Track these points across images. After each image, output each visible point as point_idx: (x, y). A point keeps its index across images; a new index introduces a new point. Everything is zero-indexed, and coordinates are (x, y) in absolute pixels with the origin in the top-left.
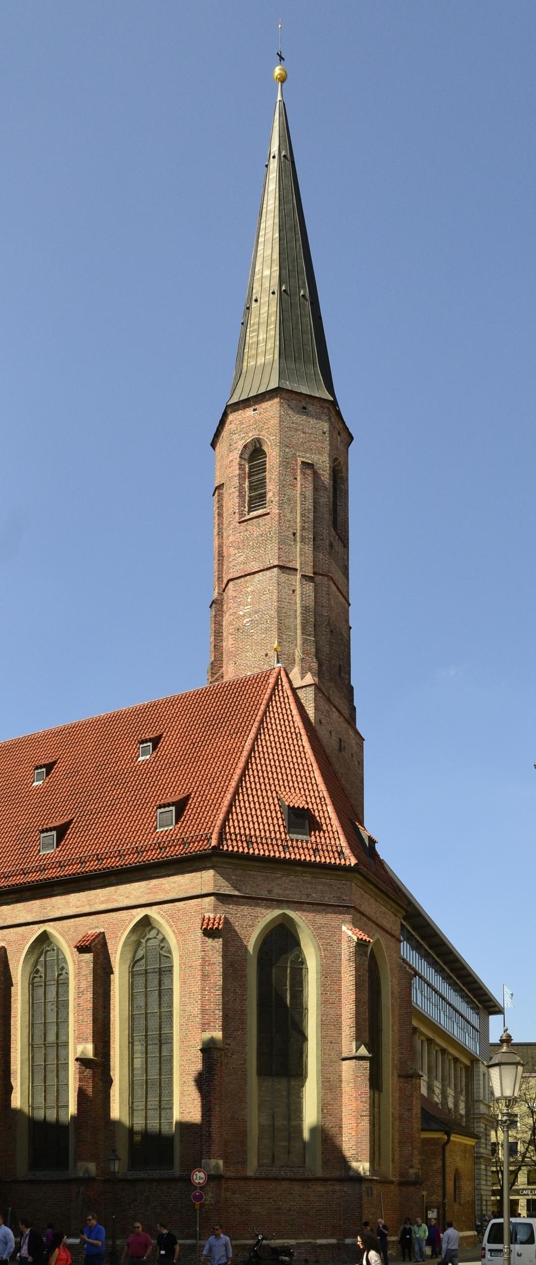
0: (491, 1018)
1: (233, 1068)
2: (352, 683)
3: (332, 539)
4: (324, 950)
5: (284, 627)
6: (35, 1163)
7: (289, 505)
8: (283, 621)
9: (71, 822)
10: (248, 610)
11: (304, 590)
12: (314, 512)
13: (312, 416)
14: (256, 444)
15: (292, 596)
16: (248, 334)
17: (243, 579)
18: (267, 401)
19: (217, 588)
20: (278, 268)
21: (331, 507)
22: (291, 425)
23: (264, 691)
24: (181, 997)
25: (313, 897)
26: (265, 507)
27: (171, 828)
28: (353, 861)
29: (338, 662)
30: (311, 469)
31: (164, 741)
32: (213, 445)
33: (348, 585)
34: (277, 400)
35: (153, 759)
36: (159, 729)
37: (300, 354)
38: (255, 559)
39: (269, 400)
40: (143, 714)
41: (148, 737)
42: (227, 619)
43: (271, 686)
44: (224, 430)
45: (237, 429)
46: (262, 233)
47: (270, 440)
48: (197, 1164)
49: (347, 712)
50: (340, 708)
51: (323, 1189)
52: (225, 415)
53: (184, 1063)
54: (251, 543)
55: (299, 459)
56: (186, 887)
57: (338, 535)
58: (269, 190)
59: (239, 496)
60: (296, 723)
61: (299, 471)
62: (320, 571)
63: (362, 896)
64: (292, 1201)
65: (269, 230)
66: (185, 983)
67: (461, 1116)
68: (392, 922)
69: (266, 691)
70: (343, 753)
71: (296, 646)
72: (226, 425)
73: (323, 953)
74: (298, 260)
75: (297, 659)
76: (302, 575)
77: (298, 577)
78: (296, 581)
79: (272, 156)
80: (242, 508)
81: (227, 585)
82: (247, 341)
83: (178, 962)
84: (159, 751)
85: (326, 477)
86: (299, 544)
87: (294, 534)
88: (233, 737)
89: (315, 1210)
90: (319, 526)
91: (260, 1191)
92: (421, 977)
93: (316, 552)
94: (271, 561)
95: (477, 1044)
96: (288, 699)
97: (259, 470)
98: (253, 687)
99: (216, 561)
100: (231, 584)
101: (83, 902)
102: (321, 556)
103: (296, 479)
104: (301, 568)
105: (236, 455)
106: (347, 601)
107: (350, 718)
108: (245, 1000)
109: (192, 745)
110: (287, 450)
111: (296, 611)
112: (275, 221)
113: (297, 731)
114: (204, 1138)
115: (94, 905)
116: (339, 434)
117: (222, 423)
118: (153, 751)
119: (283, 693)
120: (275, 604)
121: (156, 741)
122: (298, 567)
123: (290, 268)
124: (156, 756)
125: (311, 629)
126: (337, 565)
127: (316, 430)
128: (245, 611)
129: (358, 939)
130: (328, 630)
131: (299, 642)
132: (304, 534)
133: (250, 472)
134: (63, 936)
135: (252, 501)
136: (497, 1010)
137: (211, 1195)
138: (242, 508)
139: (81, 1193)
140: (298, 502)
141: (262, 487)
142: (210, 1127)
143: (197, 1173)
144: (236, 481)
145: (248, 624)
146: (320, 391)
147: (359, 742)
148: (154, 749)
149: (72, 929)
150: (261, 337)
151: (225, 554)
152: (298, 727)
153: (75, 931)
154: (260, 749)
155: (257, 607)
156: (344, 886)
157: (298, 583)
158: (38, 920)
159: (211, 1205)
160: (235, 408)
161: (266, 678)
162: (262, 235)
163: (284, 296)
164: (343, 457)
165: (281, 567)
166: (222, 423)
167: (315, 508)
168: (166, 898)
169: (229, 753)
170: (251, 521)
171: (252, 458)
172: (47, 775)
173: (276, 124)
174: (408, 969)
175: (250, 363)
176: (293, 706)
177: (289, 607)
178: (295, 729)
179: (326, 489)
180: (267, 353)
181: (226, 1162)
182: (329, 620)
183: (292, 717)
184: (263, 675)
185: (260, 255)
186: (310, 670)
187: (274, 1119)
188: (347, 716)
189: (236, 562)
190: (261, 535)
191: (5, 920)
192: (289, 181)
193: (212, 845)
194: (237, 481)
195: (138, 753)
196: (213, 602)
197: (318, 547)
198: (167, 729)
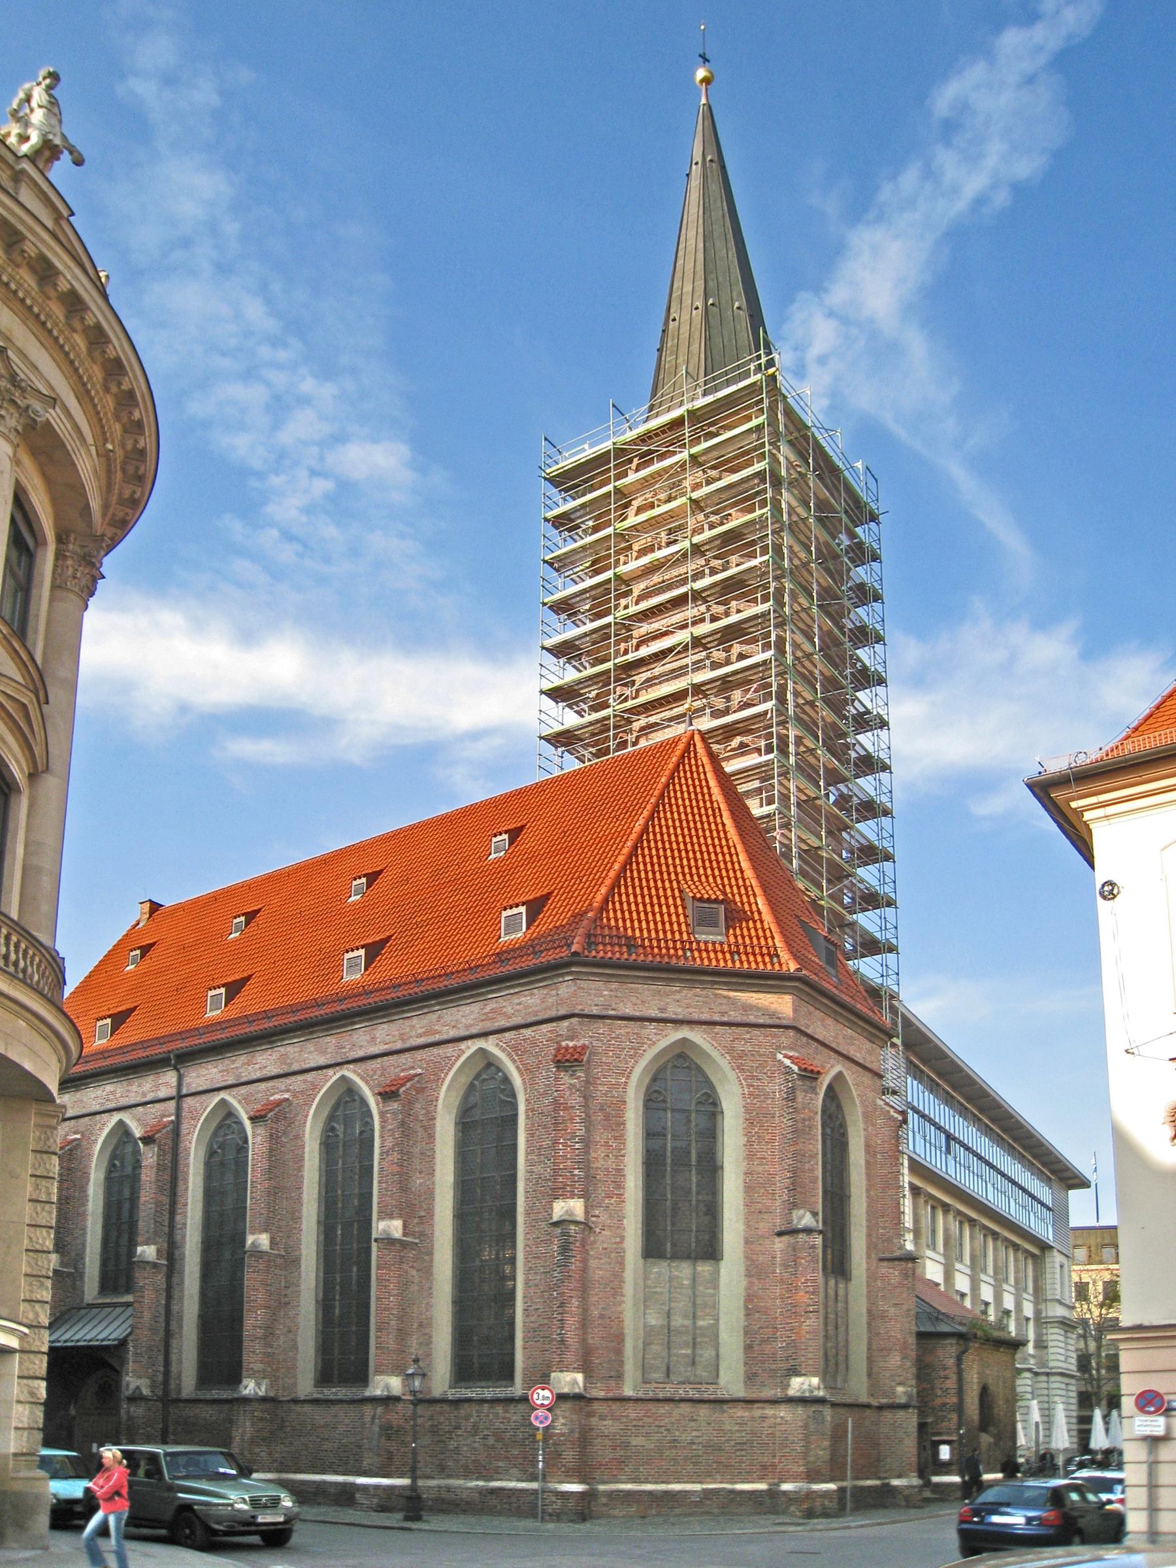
0: (1072, 1193)
4: (749, 1086)
6: (325, 1377)
24: (527, 1154)
25: (730, 1016)
28: (793, 967)
48: (544, 1380)
51: (746, 1414)
53: (529, 1243)
56: (536, 1009)
63: (810, 1013)
66: (532, 1135)
73: (746, 1090)
101: (394, 1036)
108: (623, 1156)
113: (715, 805)
115: (408, 1039)
119: (696, 760)
129: (800, 1069)
134: (367, 1082)
136: (1079, 1182)
137: (563, 1421)
142: (562, 1328)
143: (539, 1391)
149: (379, 1073)
152: (770, 929)
159: (563, 1435)
168: (508, 1025)
187: (669, 1317)
191: (290, 1065)
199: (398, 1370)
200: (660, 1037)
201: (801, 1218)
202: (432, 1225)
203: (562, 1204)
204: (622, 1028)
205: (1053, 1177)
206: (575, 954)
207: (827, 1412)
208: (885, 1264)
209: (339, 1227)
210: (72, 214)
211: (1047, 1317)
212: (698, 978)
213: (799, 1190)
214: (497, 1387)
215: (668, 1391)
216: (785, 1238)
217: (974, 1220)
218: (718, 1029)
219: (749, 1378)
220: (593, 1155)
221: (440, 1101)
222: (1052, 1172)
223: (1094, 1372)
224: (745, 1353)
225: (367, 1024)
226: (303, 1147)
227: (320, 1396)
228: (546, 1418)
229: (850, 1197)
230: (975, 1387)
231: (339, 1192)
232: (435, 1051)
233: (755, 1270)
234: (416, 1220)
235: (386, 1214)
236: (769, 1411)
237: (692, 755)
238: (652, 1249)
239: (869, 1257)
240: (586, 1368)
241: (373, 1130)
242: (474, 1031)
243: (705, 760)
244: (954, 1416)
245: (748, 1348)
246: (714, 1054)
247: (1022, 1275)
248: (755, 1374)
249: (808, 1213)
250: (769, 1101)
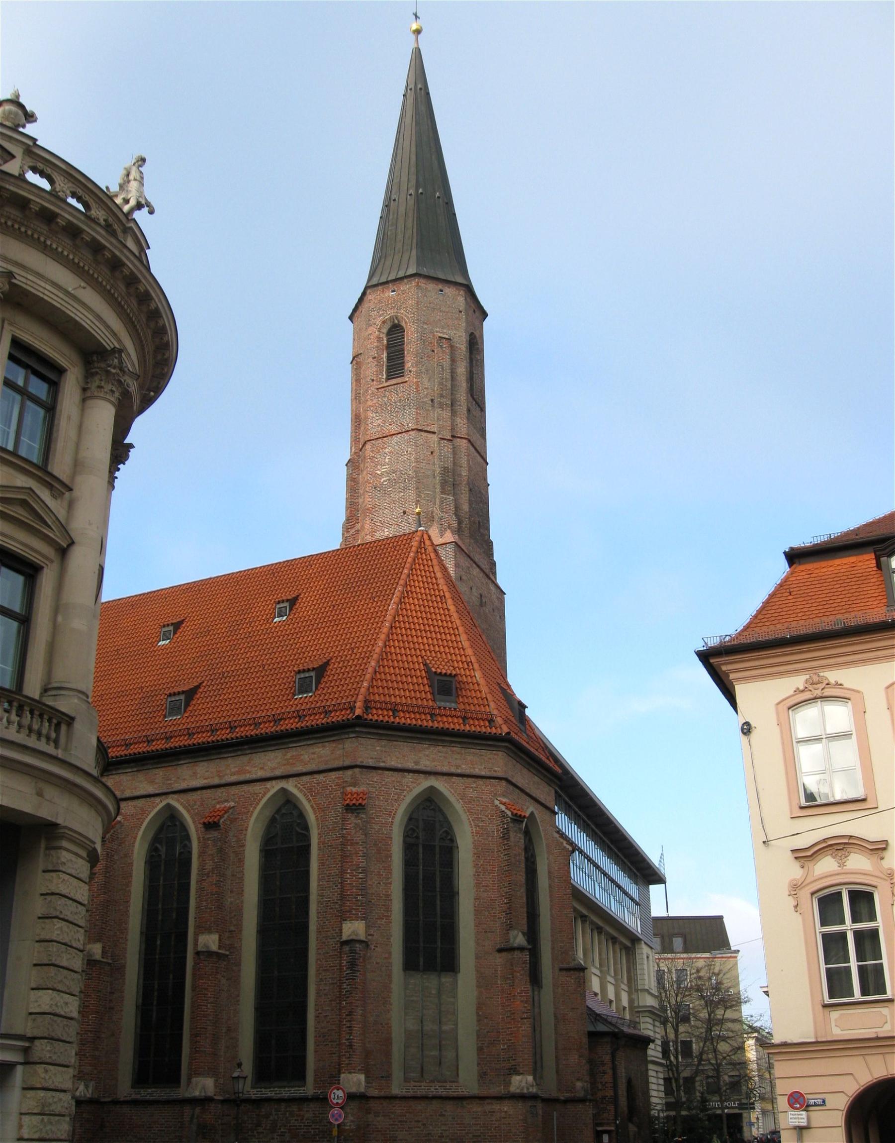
0: (652, 888)
1: (377, 963)
6: (141, 1078)
9: (198, 687)
24: (319, 880)
25: (462, 769)
26: (403, 376)
27: (310, 694)
33: (485, 446)
47: (408, 318)
50: (480, 564)
51: (479, 1109)
64: (445, 1125)
66: (323, 864)
67: (624, 1008)
68: (545, 793)
83: (317, 841)
89: (470, 1135)
91: (406, 1112)
92: (581, 852)
94: (410, 425)
95: (638, 920)
107: (489, 571)
108: (390, 884)
114: (344, 1047)
121: (293, 602)
129: (512, 813)
133: (388, 344)
134: (188, 811)
137: (352, 1118)
139: (195, 1116)
143: (335, 1091)
149: (198, 803)
153: (202, 804)
156: (496, 757)
158: (160, 791)
168: (304, 770)
171: (389, 333)
172: (175, 633)
174: (565, 845)
181: (369, 1077)
187: (422, 1022)
193: (356, 714)
199: (212, 1072)
200: (415, 785)
201: (515, 938)
202: (240, 939)
203: (349, 925)
204: (389, 777)
205: (638, 874)
206: (358, 717)
207: (540, 1105)
208: (564, 973)
209: (159, 937)
210: (149, 248)
211: (639, 1007)
212: (440, 738)
213: (514, 913)
214: (292, 1087)
215: (423, 1089)
216: (504, 954)
217: (586, 916)
218: (454, 779)
219: (481, 1077)
220: (370, 883)
221: (250, 829)
222: (638, 869)
223: (672, 1058)
224: (478, 1055)
225: (191, 761)
226: (131, 864)
227: (138, 1097)
228: (340, 1116)
229: (539, 916)
230: (624, 1081)
231: (160, 906)
232: (245, 787)
233: (483, 982)
234: (227, 934)
235: (202, 928)
236: (496, 1106)
238: (410, 965)
239: (553, 968)
240: (367, 1072)
241: (190, 853)
242: (278, 773)
244: (611, 1108)
245: (480, 1050)
246: (452, 799)
247: (604, 956)
248: (485, 1073)
249: (520, 933)
250: (490, 839)
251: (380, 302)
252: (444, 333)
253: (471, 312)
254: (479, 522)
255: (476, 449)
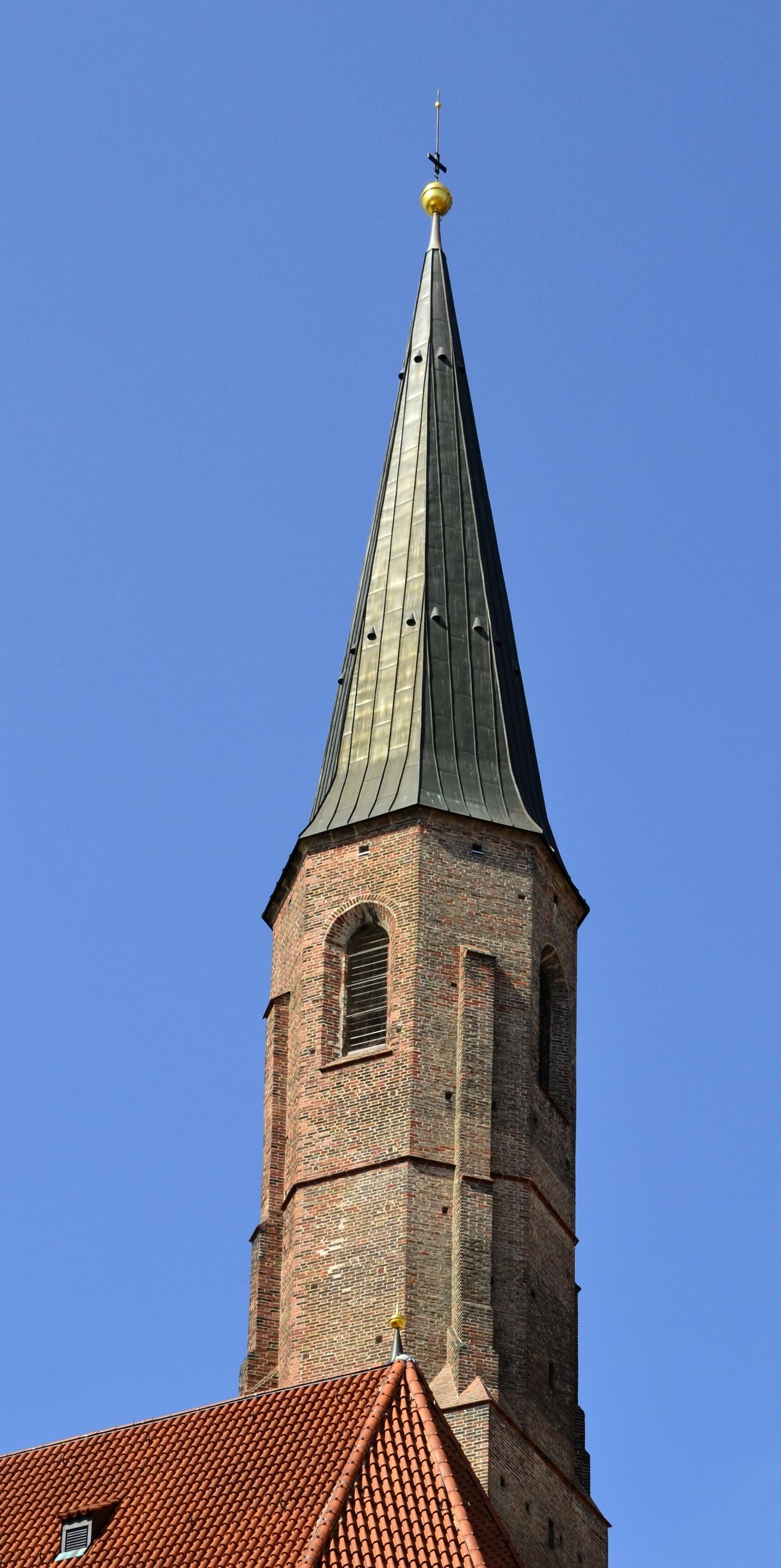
2: (581, 1403)
3: (536, 1107)
5: (422, 1284)
7: (438, 1037)
8: (419, 1270)
10: (339, 1247)
11: (469, 1207)
12: (496, 1052)
13: (494, 864)
14: (364, 917)
15: (441, 1221)
16: (352, 701)
17: (328, 1184)
18: (392, 831)
19: (267, 1202)
20: (423, 574)
21: (535, 1042)
22: (446, 879)
23: (366, 1410)
26: (383, 1042)
29: (547, 1358)
30: (488, 966)
31: (122, 1517)
32: (269, 917)
33: (572, 1201)
34: (413, 831)
35: (92, 1557)
36: (113, 1491)
37: (468, 741)
38: (357, 1144)
39: (397, 829)
40: (77, 1458)
41: (85, 1508)
42: (288, 1264)
43: (381, 1399)
44: (294, 888)
45: (322, 886)
46: (388, 506)
47: (396, 909)
49: (567, 1463)
52: (296, 859)
54: (348, 1112)
55: (462, 946)
57: (551, 1100)
58: (406, 423)
59: (324, 1017)
60: (438, 1479)
61: (461, 970)
62: (507, 1170)
65: (405, 500)
69: (370, 1411)
70: (558, 1551)
71: (448, 1321)
72: (298, 878)
74: (469, 559)
75: (450, 1349)
76: (465, 1178)
77: (456, 1181)
78: (450, 1190)
79: (413, 356)
80: (331, 1043)
81: (291, 1195)
82: (350, 715)
84: (108, 1538)
85: (523, 983)
86: (458, 1116)
87: (449, 1095)
88: (288, 1507)
90: (505, 1080)
93: (499, 1132)
94: (395, 1149)
96: (422, 1428)
97: (372, 967)
98: (340, 1402)
99: (268, 1147)
100: (300, 1195)
102: (510, 1140)
103: (454, 985)
104: (463, 1164)
105: (318, 938)
106: (571, 1233)
109: (189, 1525)
110: (436, 929)
111: (449, 1251)
112: (419, 483)
113: (441, 1496)
116: (556, 899)
117: (290, 873)
118: (92, 1540)
119: (410, 1415)
120: (402, 1235)
121: (102, 1518)
122: (456, 1161)
123: (451, 575)
124: (101, 1550)
125: (483, 1287)
126: (547, 1160)
127: (502, 890)
128: (331, 1249)
130: (524, 1291)
131: (455, 1314)
132: (471, 1096)
135: (352, 1027)
138: (331, 1043)
140: (459, 1031)
141: (377, 1001)
144: (317, 990)
145: (339, 1276)
146: (512, 815)
147: (598, 1530)
148: (96, 1535)
150: (381, 708)
151: (289, 1133)
152: (444, 1488)
154: (351, 1534)
155: (359, 1240)
157: (454, 1195)
160: (319, 844)
161: (372, 1383)
162: (388, 510)
163: (435, 627)
164: (563, 945)
165: (415, 1161)
166: (290, 873)
167: (496, 1043)
169: (276, 1543)
170: (350, 1068)
171: (352, 946)
173: (425, 294)
175: (355, 757)
176: (433, 1443)
177: (434, 1243)
178: (436, 1491)
179: (523, 1007)
180: (394, 739)
182: (527, 1270)
183: (431, 1466)
184: (366, 1378)
185: (384, 548)
186: (480, 1371)
188: (568, 1472)
189: (314, 1149)
190: (373, 1096)
192: (450, 407)
194: (321, 988)
195: (56, 1545)
196: (258, 1230)
197: (503, 1123)
198: (133, 1491)
237: (403, 1404)
243: (425, 1415)
251: (332, 874)
252: (480, 946)
253: (547, 900)
254: (551, 1366)
255: (548, 1206)
